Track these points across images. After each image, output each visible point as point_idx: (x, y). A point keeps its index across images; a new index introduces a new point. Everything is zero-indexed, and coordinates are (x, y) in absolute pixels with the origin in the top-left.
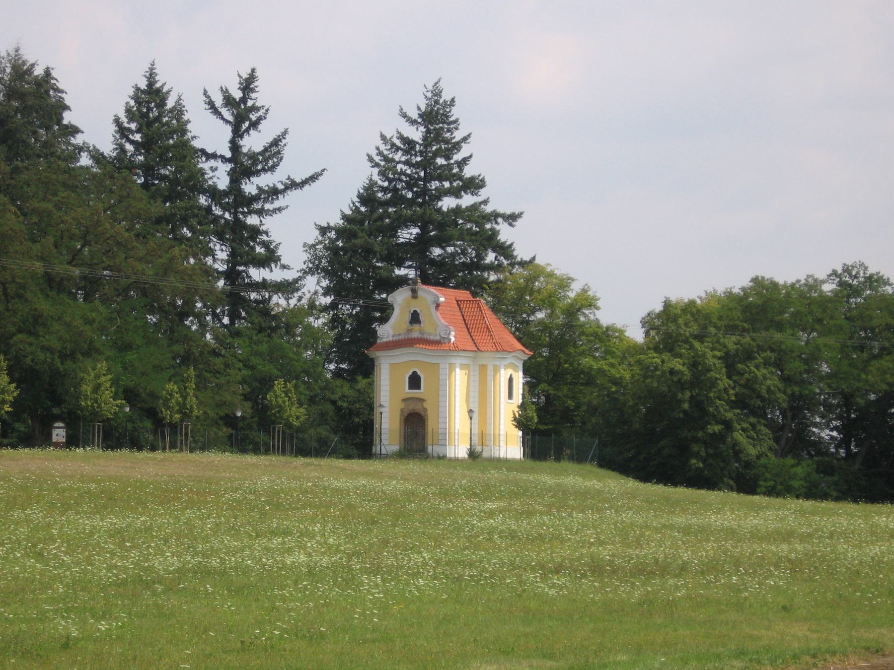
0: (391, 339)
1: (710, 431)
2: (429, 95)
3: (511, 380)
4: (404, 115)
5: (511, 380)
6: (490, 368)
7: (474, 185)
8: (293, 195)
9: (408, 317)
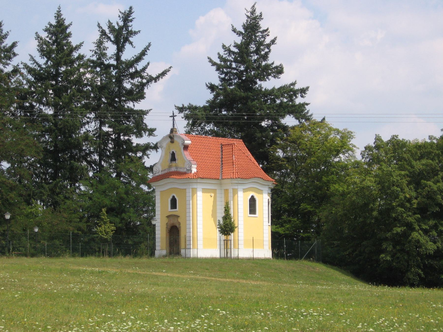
0: (160, 173)
1: (395, 232)
2: (249, 14)
3: (252, 201)
4: (234, 30)
5: (252, 201)
6: (231, 191)
7: (279, 71)
8: (153, 85)
9: (169, 157)
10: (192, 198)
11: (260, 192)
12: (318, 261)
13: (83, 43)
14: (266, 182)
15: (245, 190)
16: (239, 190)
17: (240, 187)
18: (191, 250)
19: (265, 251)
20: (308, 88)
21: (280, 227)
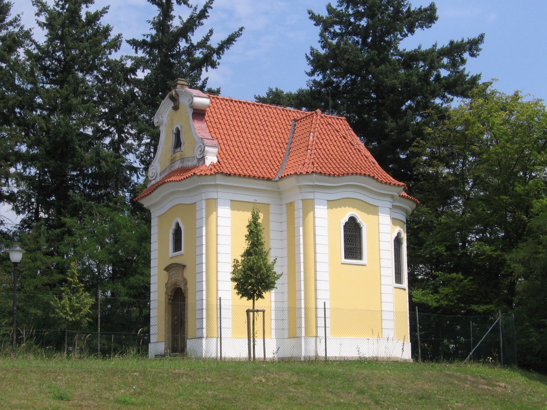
3: (353, 231)
5: (353, 231)
6: (299, 205)
10: (207, 217)
11: (373, 210)
12: (507, 362)
13: (108, 8)
14: (384, 186)
15: (332, 204)
16: (316, 201)
17: (318, 195)
18: (204, 340)
19: (393, 343)
20: (482, 37)
21: (432, 293)
